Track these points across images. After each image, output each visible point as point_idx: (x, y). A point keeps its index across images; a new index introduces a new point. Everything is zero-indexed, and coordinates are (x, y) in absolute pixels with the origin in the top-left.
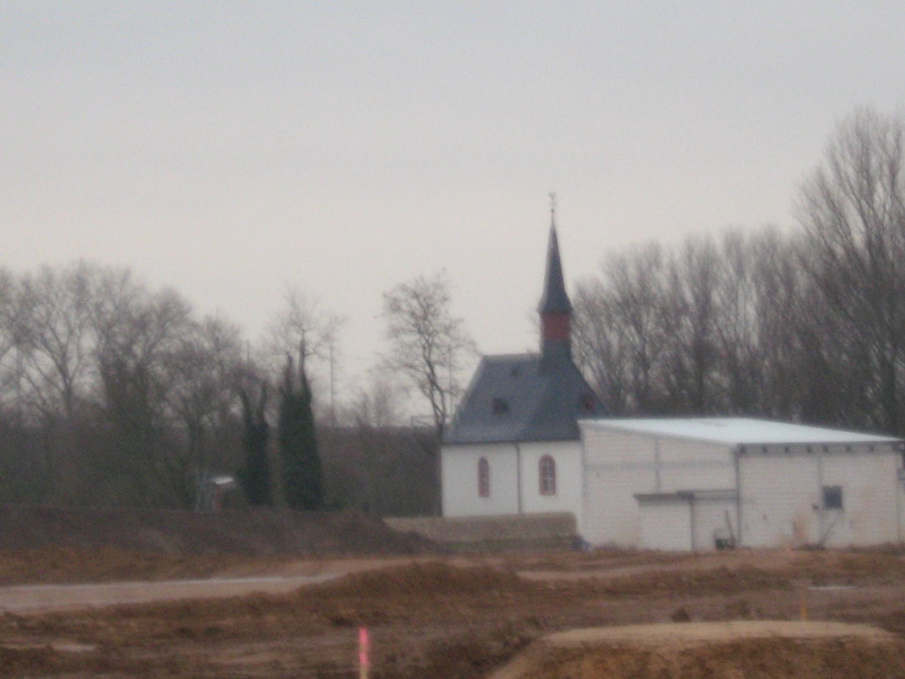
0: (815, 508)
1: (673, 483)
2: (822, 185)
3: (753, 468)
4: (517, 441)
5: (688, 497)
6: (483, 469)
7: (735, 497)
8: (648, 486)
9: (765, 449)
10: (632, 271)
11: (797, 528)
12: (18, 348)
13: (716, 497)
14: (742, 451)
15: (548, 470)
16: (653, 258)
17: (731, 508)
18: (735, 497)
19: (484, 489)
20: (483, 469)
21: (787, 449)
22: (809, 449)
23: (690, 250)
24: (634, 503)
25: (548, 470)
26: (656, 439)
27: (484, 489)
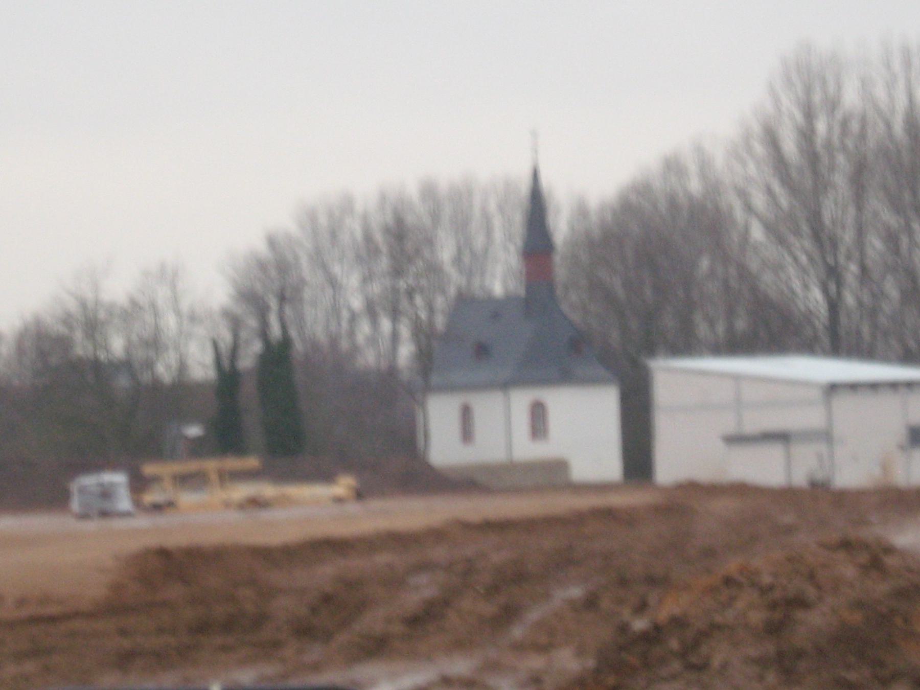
0: (901, 448)
1: (755, 423)
2: (772, 140)
3: (843, 404)
4: (506, 385)
5: (782, 437)
6: (466, 414)
7: (826, 436)
8: (729, 425)
9: (854, 387)
10: (323, 220)
11: (885, 467)
12: (490, 300)
13: (808, 436)
14: (833, 389)
15: (538, 414)
16: (347, 206)
17: (823, 448)
18: (826, 436)
19: (467, 434)
20: (466, 414)
21: (874, 386)
22: (894, 386)
23: (383, 198)
24: (721, 445)
25: (538, 414)
26: (737, 378)
27: (467, 434)
